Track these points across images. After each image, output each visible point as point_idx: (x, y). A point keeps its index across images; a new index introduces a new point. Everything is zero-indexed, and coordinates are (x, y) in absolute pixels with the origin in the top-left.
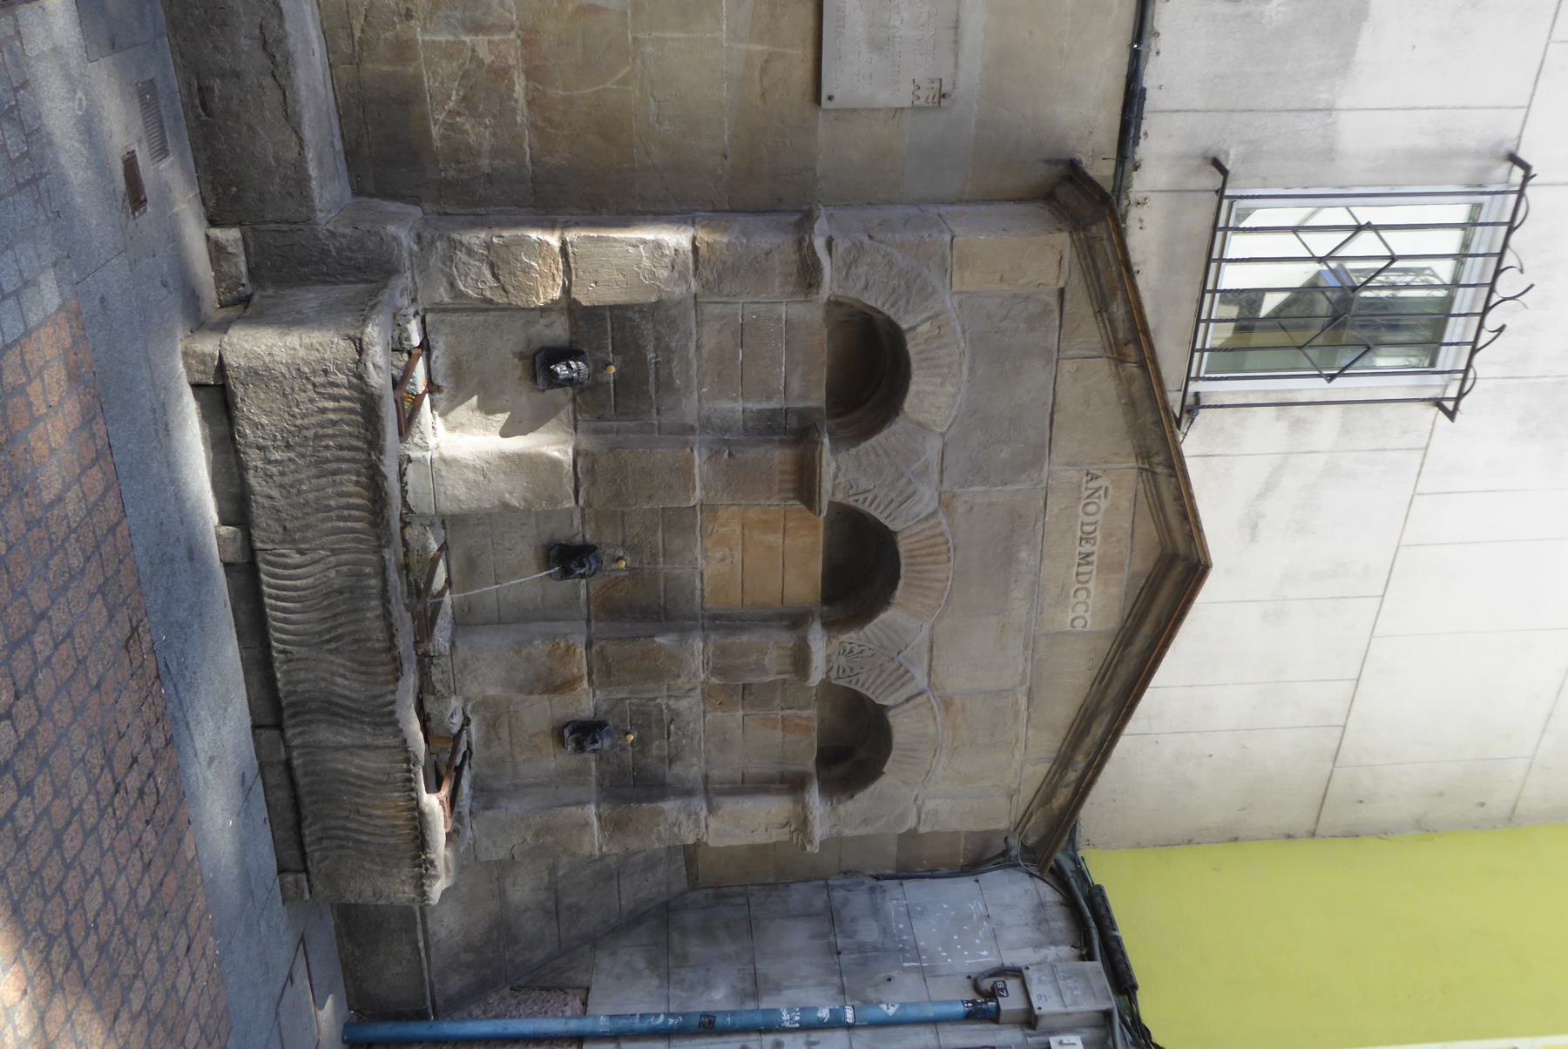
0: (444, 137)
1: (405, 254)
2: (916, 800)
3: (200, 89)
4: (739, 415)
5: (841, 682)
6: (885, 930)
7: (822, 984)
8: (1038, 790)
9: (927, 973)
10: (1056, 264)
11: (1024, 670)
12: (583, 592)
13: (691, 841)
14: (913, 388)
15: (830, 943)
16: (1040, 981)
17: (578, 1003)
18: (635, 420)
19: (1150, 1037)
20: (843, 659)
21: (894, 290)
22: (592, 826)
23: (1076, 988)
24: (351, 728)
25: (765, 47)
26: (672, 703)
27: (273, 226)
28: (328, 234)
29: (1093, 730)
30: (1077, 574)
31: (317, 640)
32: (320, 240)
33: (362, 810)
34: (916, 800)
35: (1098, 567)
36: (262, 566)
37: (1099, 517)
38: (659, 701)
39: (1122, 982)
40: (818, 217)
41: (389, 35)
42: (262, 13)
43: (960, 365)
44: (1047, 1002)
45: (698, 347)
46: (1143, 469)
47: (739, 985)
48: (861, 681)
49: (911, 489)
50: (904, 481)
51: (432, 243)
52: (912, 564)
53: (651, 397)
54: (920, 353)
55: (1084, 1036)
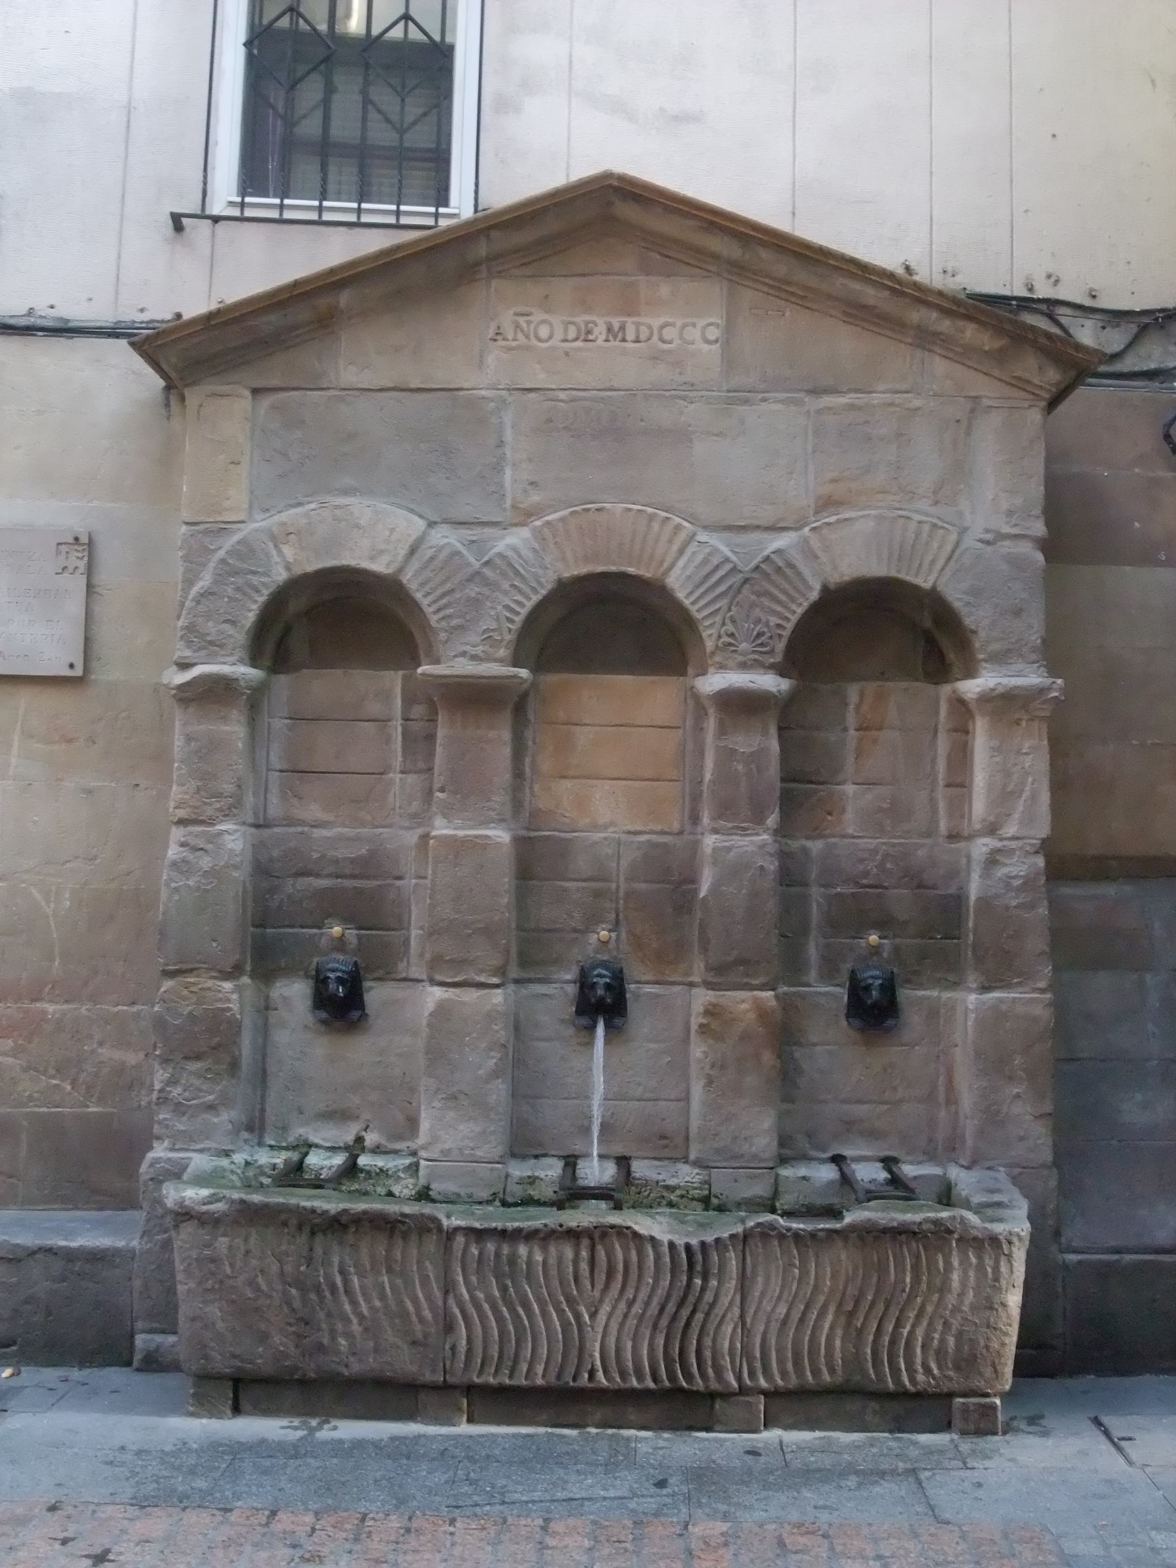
0: (101, 1100)
2: (988, 543)
4: (411, 778)
5: (780, 646)
12: (648, 989)
13: (1040, 861)
18: (409, 906)
20: (744, 646)
21: (238, 589)
22: (1001, 1000)
25: (16, 738)
28: (146, 1239)
30: (637, 341)
34: (988, 543)
35: (629, 315)
36: (465, 1380)
43: (337, 507)
48: (780, 622)
49: (498, 561)
50: (487, 572)
53: (379, 886)
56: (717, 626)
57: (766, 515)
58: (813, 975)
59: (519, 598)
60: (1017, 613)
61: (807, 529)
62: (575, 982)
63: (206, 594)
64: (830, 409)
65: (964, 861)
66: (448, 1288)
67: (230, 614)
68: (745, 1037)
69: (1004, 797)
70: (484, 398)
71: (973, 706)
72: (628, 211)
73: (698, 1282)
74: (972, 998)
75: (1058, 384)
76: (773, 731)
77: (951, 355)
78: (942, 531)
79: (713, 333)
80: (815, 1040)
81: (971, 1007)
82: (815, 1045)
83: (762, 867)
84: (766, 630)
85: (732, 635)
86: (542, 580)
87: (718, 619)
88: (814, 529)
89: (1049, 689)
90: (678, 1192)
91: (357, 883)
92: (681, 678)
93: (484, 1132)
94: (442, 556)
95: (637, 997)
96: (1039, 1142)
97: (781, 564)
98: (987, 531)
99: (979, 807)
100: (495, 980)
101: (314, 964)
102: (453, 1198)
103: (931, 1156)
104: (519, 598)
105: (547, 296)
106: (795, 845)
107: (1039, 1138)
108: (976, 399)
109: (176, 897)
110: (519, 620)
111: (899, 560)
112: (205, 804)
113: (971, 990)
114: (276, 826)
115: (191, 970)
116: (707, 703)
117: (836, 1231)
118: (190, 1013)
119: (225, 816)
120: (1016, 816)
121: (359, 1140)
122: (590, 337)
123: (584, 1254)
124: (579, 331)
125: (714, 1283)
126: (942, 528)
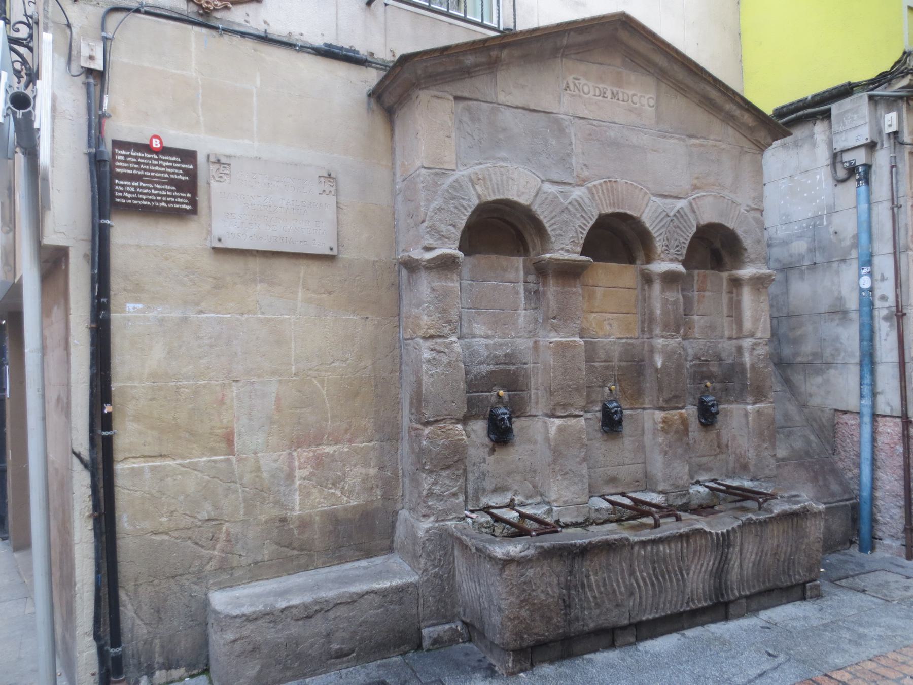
1: (436, 525)
3: (337, 657)
6: (798, 237)
7: (838, 273)
9: (832, 211)
10: (439, 101)
11: (677, 139)
14: (516, 199)
15: (808, 269)
16: (846, 140)
17: (844, 416)
19: (887, 72)
20: (672, 251)
21: (456, 207)
23: (852, 118)
24: (730, 560)
25: (300, 290)
26: (689, 358)
27: (420, 609)
30: (623, 101)
31: (681, 583)
32: (428, 580)
38: (688, 367)
39: (845, 91)
40: (410, 257)
41: (296, 532)
42: (288, 620)
43: (501, 167)
44: (864, 135)
45: (487, 337)
46: (562, 55)
47: (837, 322)
50: (570, 207)
51: (429, 507)
52: (618, 205)
54: (494, 192)
55: (883, 113)
59: (585, 222)
66: (632, 573)
69: (756, 320)
72: (624, 35)
77: (735, 127)
79: (652, 102)
85: (667, 246)
98: (747, 206)
104: (585, 222)
109: (432, 379)
113: (748, 404)
115: (442, 420)
117: (773, 517)
118: (443, 444)
121: (512, 500)
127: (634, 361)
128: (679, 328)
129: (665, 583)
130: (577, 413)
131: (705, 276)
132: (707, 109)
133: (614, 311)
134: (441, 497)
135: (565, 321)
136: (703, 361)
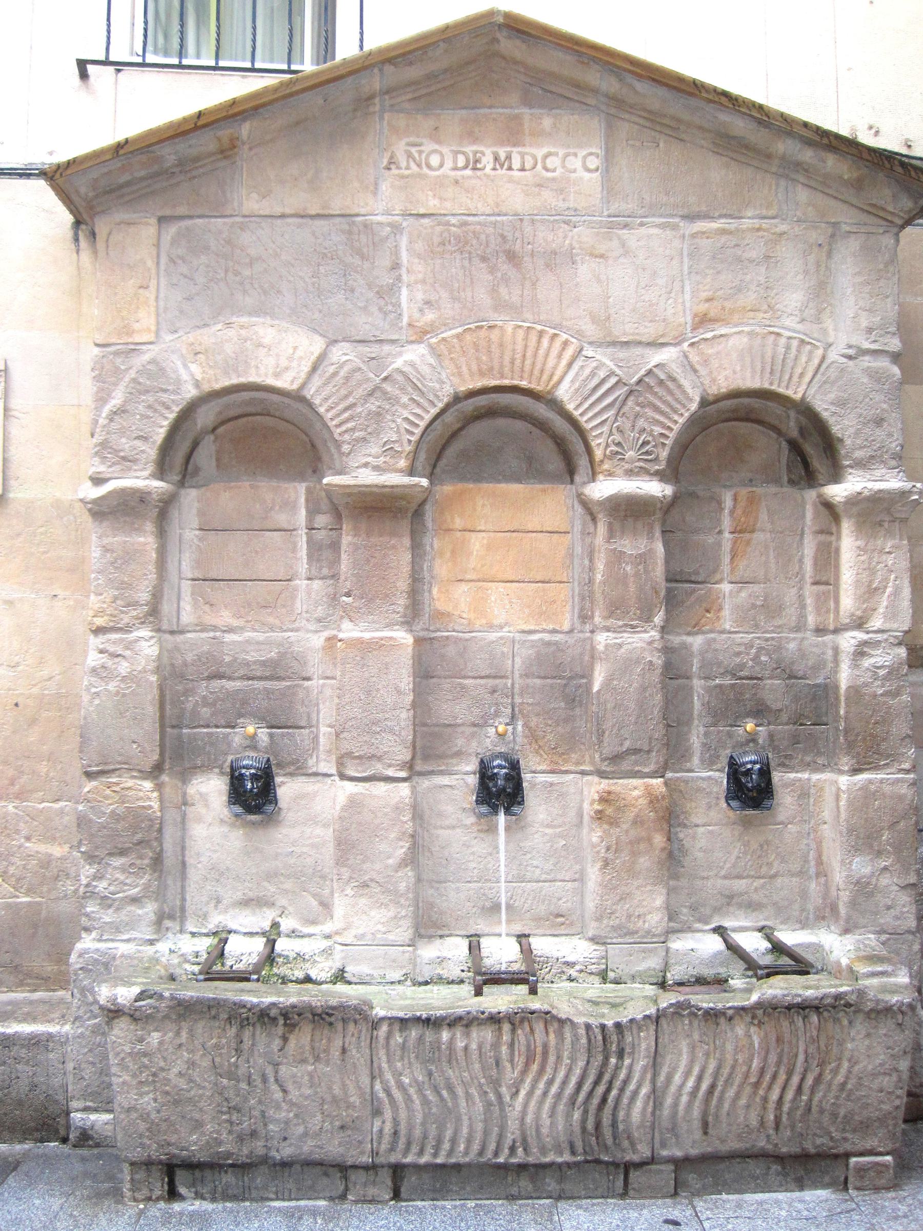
0: (29, 892)
2: (850, 357)
4: (317, 584)
5: (664, 454)
8: (836, 198)
12: (541, 778)
13: (902, 652)
18: (318, 705)
20: (631, 454)
21: (150, 407)
22: (870, 782)
28: (77, 1024)
29: (736, 132)
30: (523, 169)
33: (753, 1080)
34: (850, 357)
35: (514, 146)
36: (393, 1158)
37: (445, 150)
43: (242, 327)
49: (400, 378)
50: (387, 387)
53: (289, 687)
56: (605, 436)
57: (648, 331)
58: (696, 760)
59: (418, 411)
60: (879, 422)
61: (686, 344)
62: (475, 773)
63: (120, 411)
64: (704, 233)
65: (830, 652)
67: (141, 430)
68: (638, 821)
69: (870, 592)
70: (379, 223)
71: (840, 510)
73: (613, 1060)
74: (844, 781)
75: (910, 211)
76: (658, 534)
77: (813, 184)
78: (809, 347)
79: (593, 163)
80: (699, 822)
81: (843, 788)
82: (697, 826)
83: (651, 662)
84: (650, 439)
85: (619, 444)
86: (439, 393)
87: (605, 429)
88: (692, 345)
89: (910, 492)
90: (578, 967)
91: (268, 684)
92: (569, 486)
93: (395, 917)
94: (342, 373)
95: (533, 785)
96: (905, 910)
97: (663, 377)
98: (850, 347)
99: (848, 602)
100: (403, 774)
101: (229, 761)
102: (367, 979)
103: (804, 924)
104: (418, 411)
105: (436, 128)
106: (676, 640)
107: (904, 906)
108: (835, 225)
109: (97, 702)
110: (418, 431)
111: (772, 373)
112: (123, 612)
113: (841, 772)
114: (189, 631)
115: (114, 770)
116: (595, 509)
118: (113, 812)
119: (143, 623)
120: (881, 610)
121: (275, 925)
122: (479, 166)
123: (506, 1037)
124: (468, 161)
125: (627, 1062)
126: (809, 343)
127: (563, 678)
128: (650, 610)
129: (456, 1105)
130: (390, 772)
131: (752, 500)
132: (734, 155)
133: (513, 578)
134: (109, 902)
135: (371, 600)
136: (741, 678)
